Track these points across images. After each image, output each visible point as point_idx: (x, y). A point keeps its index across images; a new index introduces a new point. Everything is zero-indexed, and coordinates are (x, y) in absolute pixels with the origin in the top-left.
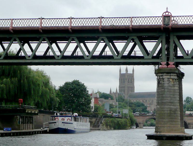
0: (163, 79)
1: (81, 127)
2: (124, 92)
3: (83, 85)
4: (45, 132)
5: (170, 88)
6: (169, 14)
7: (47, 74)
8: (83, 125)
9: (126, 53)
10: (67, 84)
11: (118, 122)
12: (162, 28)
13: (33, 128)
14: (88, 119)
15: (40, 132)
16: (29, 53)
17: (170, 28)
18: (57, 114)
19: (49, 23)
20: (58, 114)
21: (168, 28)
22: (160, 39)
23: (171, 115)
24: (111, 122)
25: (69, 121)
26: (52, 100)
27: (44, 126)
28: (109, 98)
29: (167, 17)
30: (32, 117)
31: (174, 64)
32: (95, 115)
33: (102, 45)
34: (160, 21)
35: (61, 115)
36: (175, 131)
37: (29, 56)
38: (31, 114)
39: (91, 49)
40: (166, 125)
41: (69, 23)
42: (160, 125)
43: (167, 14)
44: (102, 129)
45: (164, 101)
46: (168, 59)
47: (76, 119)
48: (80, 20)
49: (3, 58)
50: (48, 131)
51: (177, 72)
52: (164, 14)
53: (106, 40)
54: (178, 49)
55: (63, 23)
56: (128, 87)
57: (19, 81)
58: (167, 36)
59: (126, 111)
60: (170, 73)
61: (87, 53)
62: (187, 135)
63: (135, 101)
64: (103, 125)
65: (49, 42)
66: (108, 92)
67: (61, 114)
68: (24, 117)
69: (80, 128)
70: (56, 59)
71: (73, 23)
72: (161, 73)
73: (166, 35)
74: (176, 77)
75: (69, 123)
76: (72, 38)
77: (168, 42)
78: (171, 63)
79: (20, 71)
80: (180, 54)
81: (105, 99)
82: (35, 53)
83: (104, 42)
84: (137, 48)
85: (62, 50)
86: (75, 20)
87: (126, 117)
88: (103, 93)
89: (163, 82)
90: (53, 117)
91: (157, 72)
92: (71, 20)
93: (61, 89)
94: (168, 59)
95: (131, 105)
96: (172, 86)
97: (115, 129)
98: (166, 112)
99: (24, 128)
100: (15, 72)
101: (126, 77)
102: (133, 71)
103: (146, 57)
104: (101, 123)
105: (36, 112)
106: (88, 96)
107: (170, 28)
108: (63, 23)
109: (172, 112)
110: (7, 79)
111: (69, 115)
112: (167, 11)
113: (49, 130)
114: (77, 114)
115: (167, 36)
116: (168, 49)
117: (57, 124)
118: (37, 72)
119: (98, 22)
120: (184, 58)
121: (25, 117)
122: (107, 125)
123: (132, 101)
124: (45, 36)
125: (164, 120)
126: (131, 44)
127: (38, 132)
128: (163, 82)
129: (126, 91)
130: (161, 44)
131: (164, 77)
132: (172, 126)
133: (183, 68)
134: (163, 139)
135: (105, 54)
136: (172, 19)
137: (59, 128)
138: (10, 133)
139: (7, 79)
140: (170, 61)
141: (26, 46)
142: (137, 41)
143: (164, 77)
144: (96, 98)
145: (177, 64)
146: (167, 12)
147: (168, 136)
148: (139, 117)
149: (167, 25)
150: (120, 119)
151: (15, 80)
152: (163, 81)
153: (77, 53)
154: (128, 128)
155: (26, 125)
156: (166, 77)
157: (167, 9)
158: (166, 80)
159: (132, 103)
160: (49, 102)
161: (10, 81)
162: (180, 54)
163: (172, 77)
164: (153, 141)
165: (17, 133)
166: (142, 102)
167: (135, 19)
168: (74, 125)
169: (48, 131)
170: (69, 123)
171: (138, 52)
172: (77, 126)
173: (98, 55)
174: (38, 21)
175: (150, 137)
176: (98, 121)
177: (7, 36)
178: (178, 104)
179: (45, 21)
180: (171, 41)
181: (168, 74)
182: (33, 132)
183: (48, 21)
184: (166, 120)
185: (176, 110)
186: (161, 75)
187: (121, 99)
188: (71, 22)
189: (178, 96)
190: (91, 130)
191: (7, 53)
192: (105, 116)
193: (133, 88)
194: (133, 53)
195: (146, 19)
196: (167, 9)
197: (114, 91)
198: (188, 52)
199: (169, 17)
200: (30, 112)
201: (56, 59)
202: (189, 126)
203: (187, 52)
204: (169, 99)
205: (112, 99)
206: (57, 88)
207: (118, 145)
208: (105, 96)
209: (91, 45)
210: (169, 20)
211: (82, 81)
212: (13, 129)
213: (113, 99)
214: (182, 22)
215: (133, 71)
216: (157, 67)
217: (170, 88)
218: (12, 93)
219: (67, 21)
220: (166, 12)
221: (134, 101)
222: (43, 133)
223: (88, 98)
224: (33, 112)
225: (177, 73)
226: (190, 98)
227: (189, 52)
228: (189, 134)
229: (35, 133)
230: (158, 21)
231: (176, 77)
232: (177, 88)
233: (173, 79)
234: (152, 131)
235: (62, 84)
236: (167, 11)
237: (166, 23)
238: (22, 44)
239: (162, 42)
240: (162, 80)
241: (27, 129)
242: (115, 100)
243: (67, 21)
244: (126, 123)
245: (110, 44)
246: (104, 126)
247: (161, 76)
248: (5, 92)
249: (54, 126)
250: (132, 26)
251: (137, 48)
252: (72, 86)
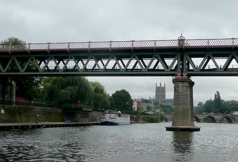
0: (179, 86)
1: (123, 121)
2: (159, 99)
3: (128, 93)
4: (98, 124)
5: (183, 93)
6: (183, 38)
7: (102, 85)
8: (124, 120)
10: (117, 92)
11: (152, 118)
12: (178, 48)
13: (88, 121)
14: (129, 116)
15: (94, 124)
16: (102, 67)
17: (184, 49)
18: (106, 112)
19: (95, 45)
20: (107, 112)
21: (182, 49)
22: (176, 57)
23: (184, 113)
24: (147, 118)
25: (114, 117)
26: (106, 102)
27: (97, 120)
28: (149, 103)
29: (181, 40)
30: (88, 114)
31: (186, 75)
32: (136, 113)
33: (133, 62)
34: (176, 43)
35: (109, 112)
36: (187, 125)
37: (102, 69)
38: (87, 111)
39: (147, 64)
40: (180, 120)
41: (109, 45)
42: (175, 120)
43: (181, 38)
44: (140, 122)
45: (179, 103)
46: (182, 71)
47: (119, 115)
48: (117, 43)
50: (100, 123)
51: (189, 81)
52: (179, 38)
53: (137, 58)
54: (190, 64)
55: (105, 45)
56: (161, 95)
57: (79, 88)
58: (182, 54)
59: (158, 111)
60: (184, 82)
61: (123, 67)
62: (196, 128)
63: (166, 104)
64: (141, 120)
65: (95, 59)
66: (149, 99)
67: (109, 112)
68: (81, 114)
69: (126, 122)
71: (113, 45)
72: (177, 82)
73: (181, 54)
74: (188, 85)
75: (114, 118)
77: (182, 59)
78: (184, 74)
79: (80, 81)
80: (191, 68)
81: (146, 103)
83: (136, 59)
84: (160, 64)
85: (105, 65)
86: (114, 43)
87: (158, 115)
88: (145, 99)
89: (178, 89)
90: (103, 113)
91: (174, 81)
92: (111, 43)
93: (113, 95)
94: (182, 71)
95: (162, 106)
96: (185, 91)
97: (150, 122)
98: (180, 111)
99: (86, 121)
100: (76, 82)
101: (160, 89)
102: (165, 85)
103: (166, 70)
104: (140, 118)
105: (91, 110)
106: (132, 100)
107: (184, 49)
108: (105, 45)
109: (185, 111)
110: (71, 87)
111: (115, 113)
113: (101, 123)
114: (120, 112)
115: (182, 54)
116: (182, 64)
117: (106, 118)
118: (94, 84)
119: (131, 44)
121: (82, 114)
122: (144, 120)
123: (164, 105)
125: (179, 117)
126: (155, 61)
127: (92, 124)
128: (178, 89)
129: (160, 98)
130: (177, 60)
131: (179, 84)
132: (185, 121)
133: (193, 79)
134: (177, 131)
136: (185, 41)
137: (107, 122)
138: (70, 125)
139: (71, 87)
140: (184, 73)
141: (80, 63)
142: (159, 58)
143: (179, 84)
144: (138, 103)
145: (189, 76)
146: (181, 36)
147: (181, 128)
148: (167, 115)
149: (181, 46)
150: (153, 116)
151: (77, 87)
152: (179, 88)
154: (159, 122)
155: (81, 119)
156: (180, 84)
157: (181, 34)
158: (180, 87)
159: (164, 106)
161: (72, 88)
162: (191, 68)
163: (185, 85)
164: (171, 132)
165: (75, 124)
166: (170, 105)
167: (158, 42)
168: (118, 120)
169: (100, 123)
170: (114, 118)
171: (160, 66)
172: (120, 120)
173: (132, 68)
174: (87, 44)
175: (168, 129)
176: (138, 117)
177: (66, 55)
178: (190, 105)
179: (92, 44)
180: (185, 59)
181: (182, 83)
182: (88, 124)
183: (94, 44)
184: (180, 117)
185: (188, 109)
186: (177, 83)
187: (156, 103)
188: (111, 45)
189: (190, 99)
190: (131, 123)
191: (66, 67)
192: (144, 114)
193: (165, 96)
195: (166, 42)
196: (181, 34)
197: (152, 97)
198: (197, 66)
199: (183, 40)
200: (85, 110)
202: (200, 121)
203: (196, 67)
204: (183, 101)
205: (151, 103)
206: (111, 95)
207: (56, 160)
208: (146, 101)
209: (147, 62)
210: (183, 42)
211: (127, 90)
212: (71, 122)
213: (152, 103)
214: (33, 48)
215: (165, 85)
216: (174, 77)
217: (183, 93)
218: (74, 97)
219: (108, 43)
220: (180, 37)
221: (165, 104)
222: (95, 125)
223: (131, 102)
224: (88, 110)
225: (188, 82)
226: (201, 103)
227: (198, 67)
228: (197, 127)
229: (92, 125)
230: (174, 43)
231: (188, 84)
232: (188, 93)
233: (186, 86)
234: (170, 124)
235: (114, 92)
237: (181, 44)
238: (77, 61)
239: (177, 59)
240: (177, 87)
241: (83, 122)
242: (153, 104)
243: (108, 43)
244: (158, 118)
246: (142, 120)
247: (177, 84)
249: (104, 120)
250: (156, 47)
251: (160, 64)
252: (121, 94)
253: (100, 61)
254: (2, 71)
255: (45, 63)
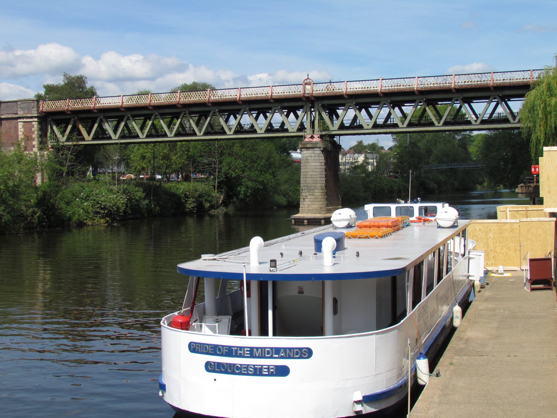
9: (486, 117)
49: (480, 123)
52: (306, 81)
70: (227, 134)
76: (493, 96)
82: (376, 120)
112: (308, 78)
120: (257, 132)
124: (458, 95)
126: (493, 104)
135: (391, 121)
146: (308, 78)
153: (358, 121)
157: (308, 75)
160: (425, 175)
194: (424, 119)
201: (227, 134)
220: (307, 79)
236: (308, 78)
245: (503, 102)
248: (357, 164)
253: (397, 109)
254: (141, 138)
255: (266, 117)
